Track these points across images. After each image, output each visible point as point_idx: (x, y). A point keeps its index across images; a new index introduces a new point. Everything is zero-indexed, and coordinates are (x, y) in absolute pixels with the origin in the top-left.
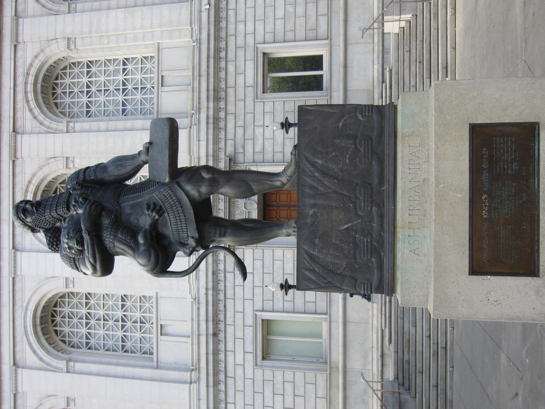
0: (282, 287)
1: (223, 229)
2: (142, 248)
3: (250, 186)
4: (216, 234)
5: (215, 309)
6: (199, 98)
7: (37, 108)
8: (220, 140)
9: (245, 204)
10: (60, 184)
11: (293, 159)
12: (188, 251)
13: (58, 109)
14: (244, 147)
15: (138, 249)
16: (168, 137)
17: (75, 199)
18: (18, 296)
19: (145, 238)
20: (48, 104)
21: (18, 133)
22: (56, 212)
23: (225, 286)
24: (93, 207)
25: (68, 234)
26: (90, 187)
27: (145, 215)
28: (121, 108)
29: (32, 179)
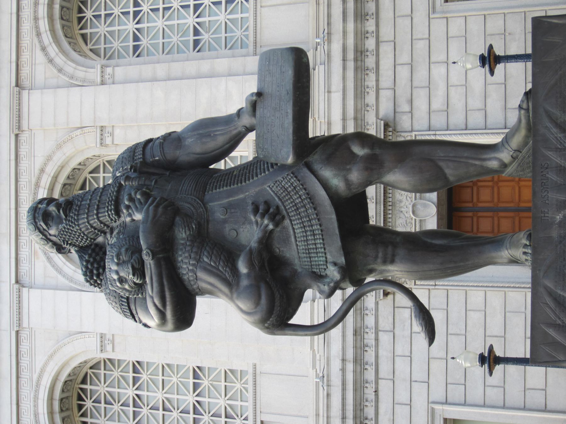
0: (482, 359)
1: (390, 249)
2: (245, 282)
3: (440, 169)
4: (376, 257)
5: (358, 397)
6: (329, 16)
7: (53, 44)
8: (367, 90)
9: (414, 206)
10: (90, 173)
11: (523, 118)
12: (326, 288)
13: (87, 44)
14: (411, 102)
15: (238, 284)
16: (291, 82)
17: (130, 195)
18: (24, 362)
19: (251, 264)
20: (71, 38)
21: (23, 89)
22: (98, 218)
23: (377, 357)
24: (160, 210)
25: (118, 256)
26: (154, 174)
27: (250, 223)
28: (192, 38)
29: (45, 164)
